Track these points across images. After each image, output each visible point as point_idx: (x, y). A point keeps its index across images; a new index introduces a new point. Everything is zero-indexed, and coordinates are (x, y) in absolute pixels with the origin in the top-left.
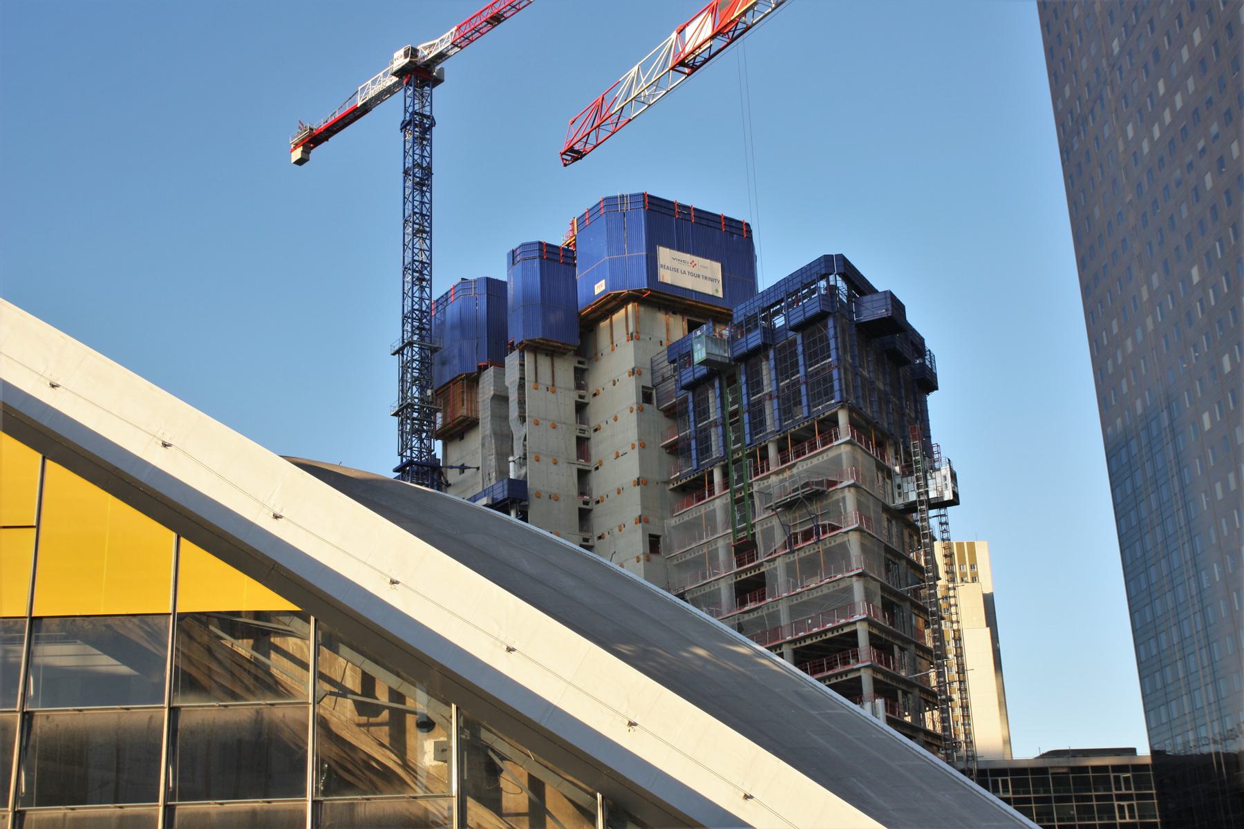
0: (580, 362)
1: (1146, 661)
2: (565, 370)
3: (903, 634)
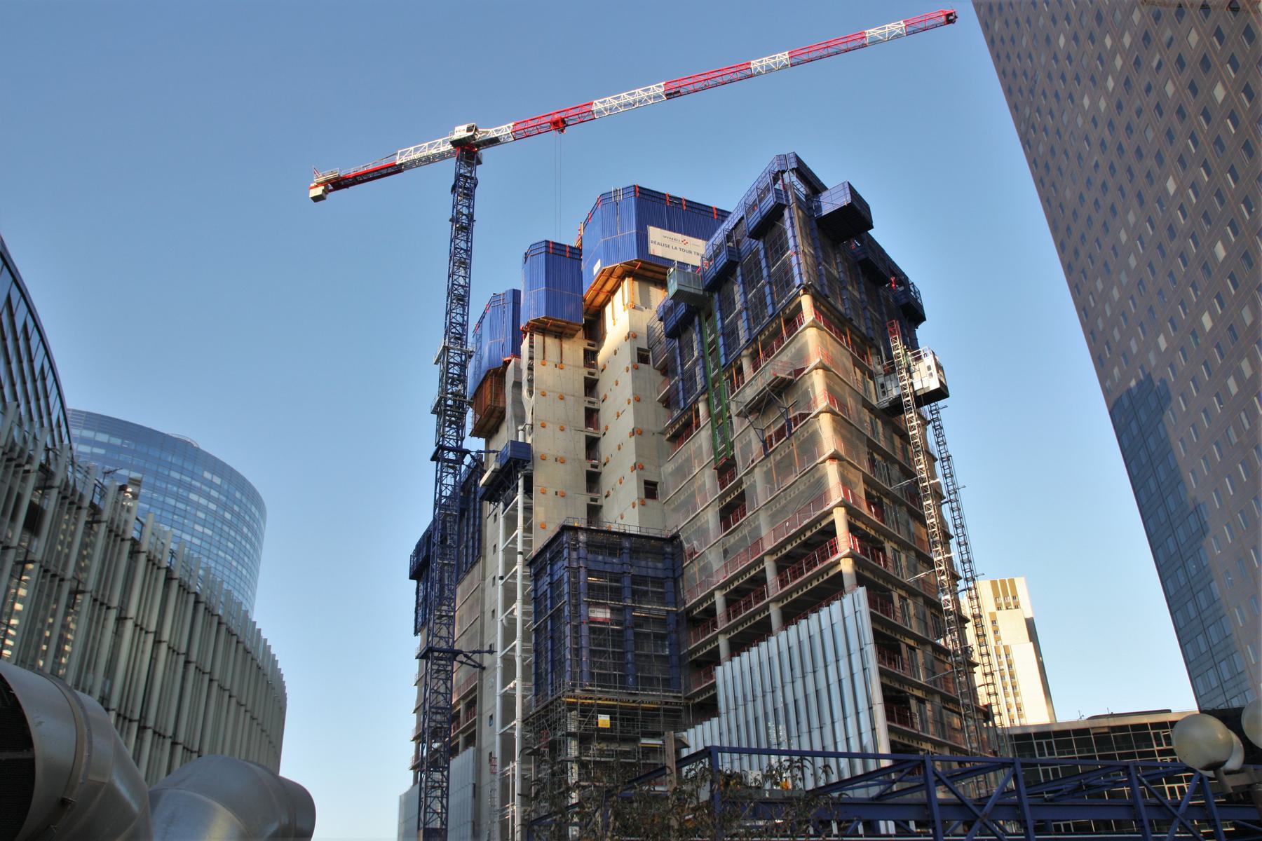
0: (589, 345)
1: (1175, 594)
2: (575, 349)
3: (896, 533)
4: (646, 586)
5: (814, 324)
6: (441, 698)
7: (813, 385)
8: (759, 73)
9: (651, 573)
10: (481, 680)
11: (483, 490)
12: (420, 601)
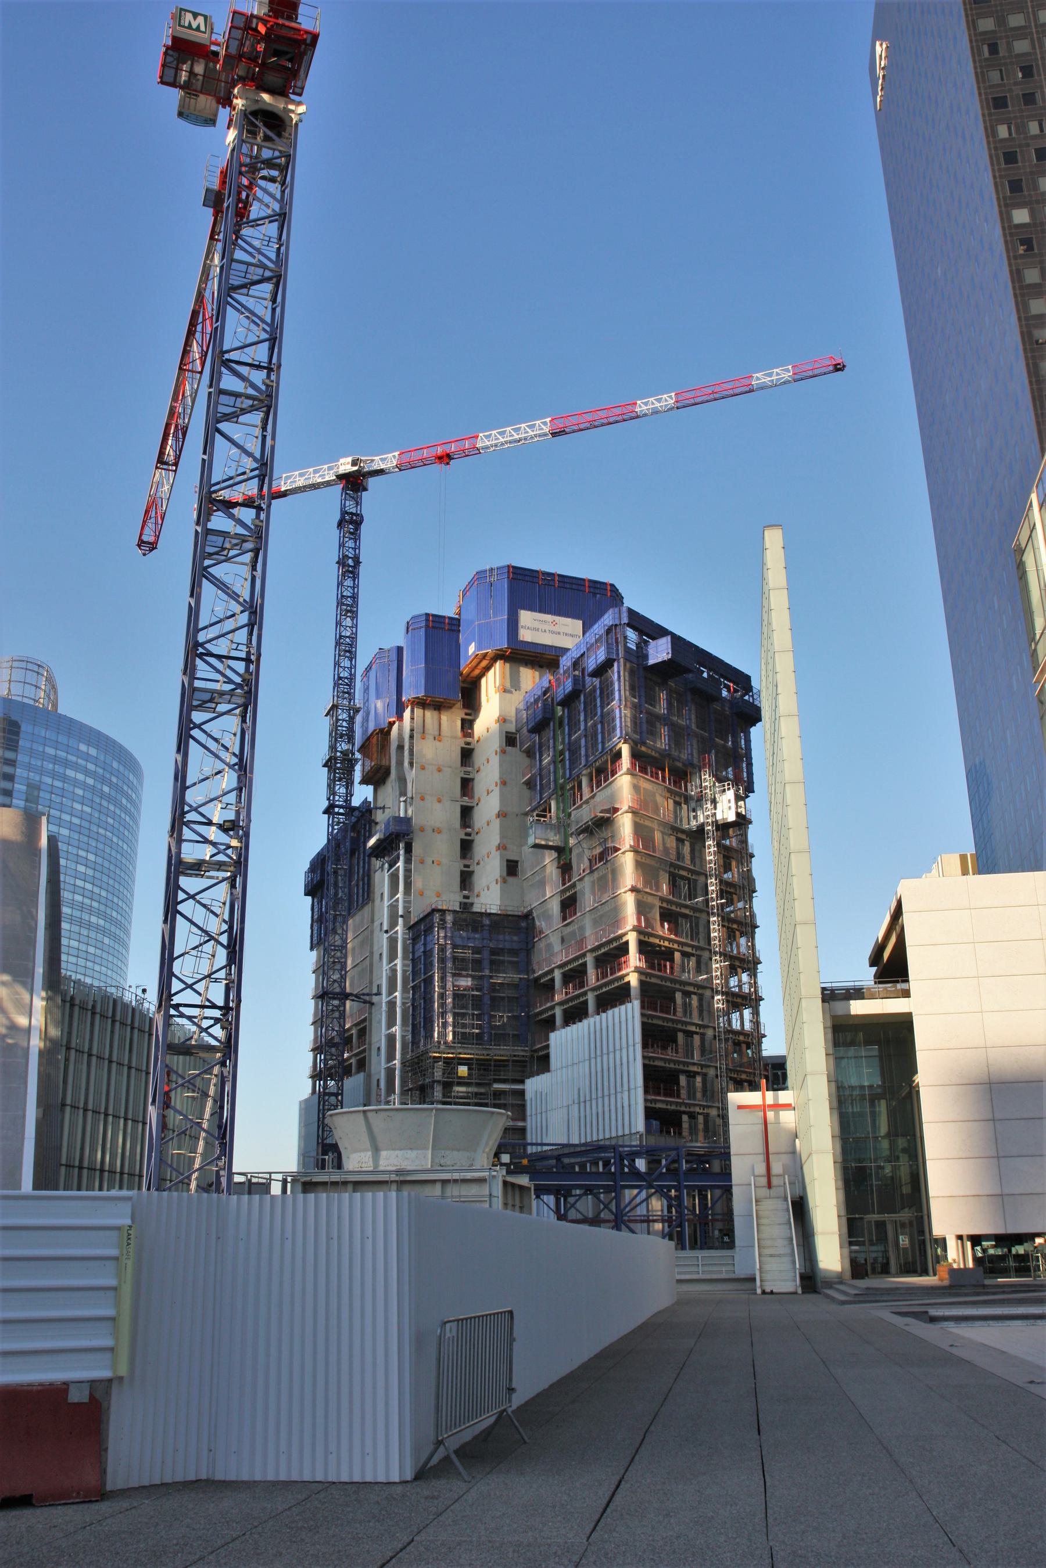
0: (466, 714)
2: (451, 721)
4: (504, 956)
5: (629, 772)
6: (336, 985)
7: (623, 824)
8: (645, 415)
9: (508, 946)
10: (370, 1013)
11: (371, 851)
12: (316, 917)
